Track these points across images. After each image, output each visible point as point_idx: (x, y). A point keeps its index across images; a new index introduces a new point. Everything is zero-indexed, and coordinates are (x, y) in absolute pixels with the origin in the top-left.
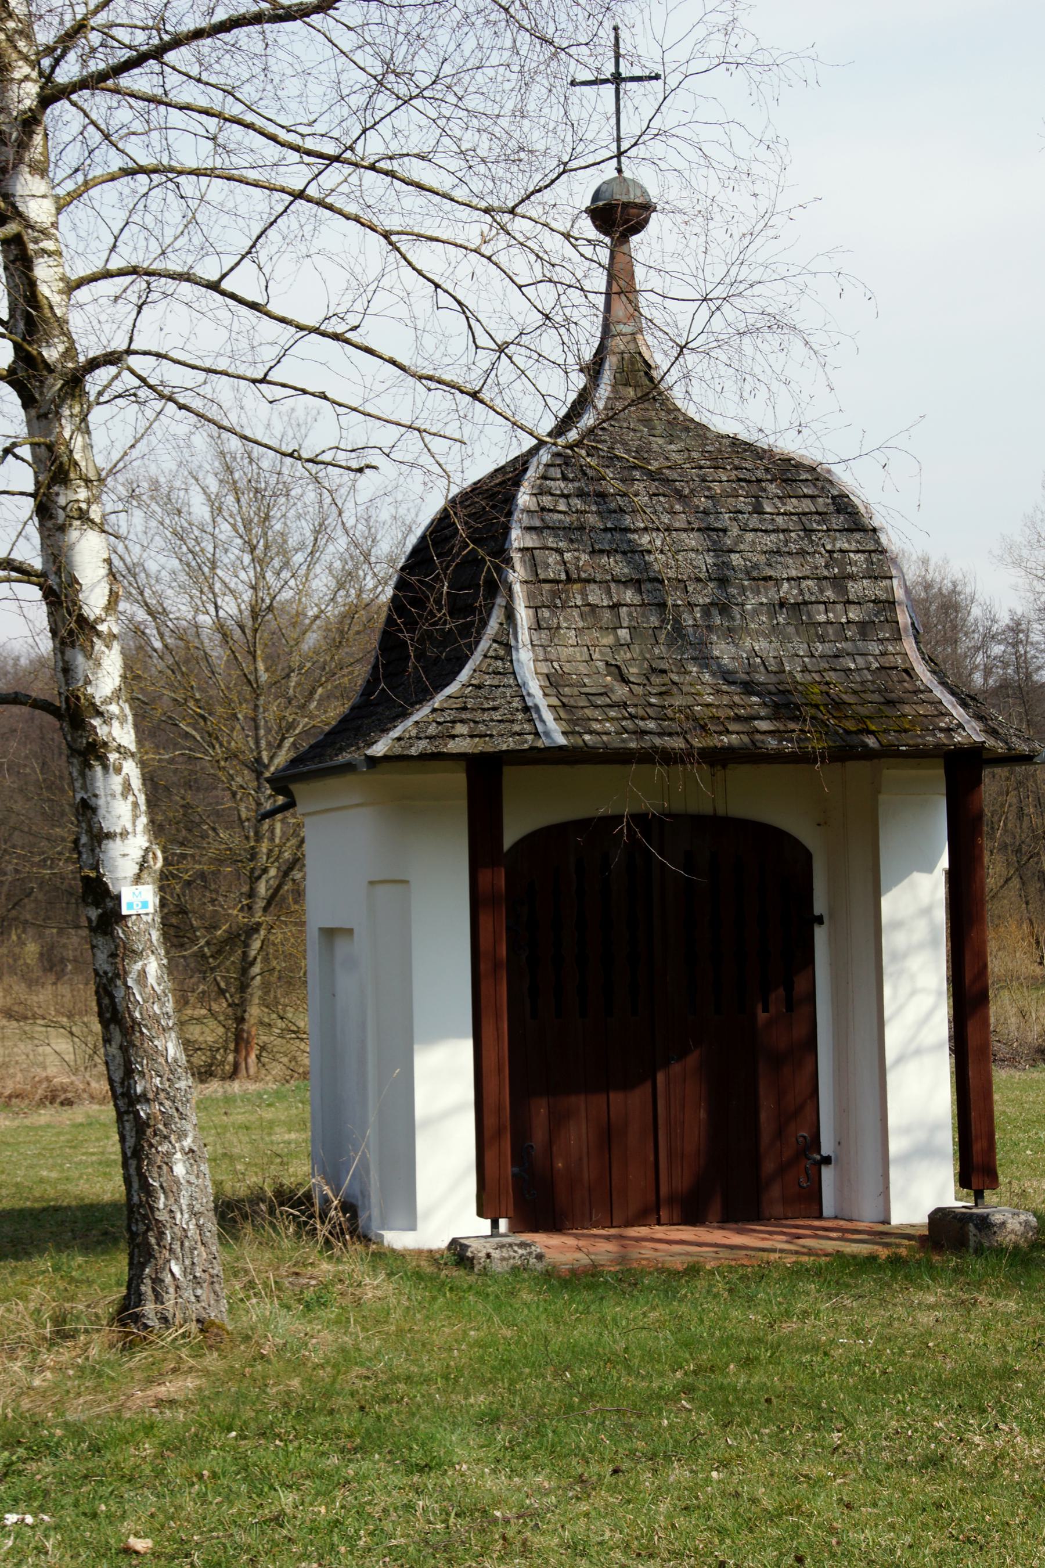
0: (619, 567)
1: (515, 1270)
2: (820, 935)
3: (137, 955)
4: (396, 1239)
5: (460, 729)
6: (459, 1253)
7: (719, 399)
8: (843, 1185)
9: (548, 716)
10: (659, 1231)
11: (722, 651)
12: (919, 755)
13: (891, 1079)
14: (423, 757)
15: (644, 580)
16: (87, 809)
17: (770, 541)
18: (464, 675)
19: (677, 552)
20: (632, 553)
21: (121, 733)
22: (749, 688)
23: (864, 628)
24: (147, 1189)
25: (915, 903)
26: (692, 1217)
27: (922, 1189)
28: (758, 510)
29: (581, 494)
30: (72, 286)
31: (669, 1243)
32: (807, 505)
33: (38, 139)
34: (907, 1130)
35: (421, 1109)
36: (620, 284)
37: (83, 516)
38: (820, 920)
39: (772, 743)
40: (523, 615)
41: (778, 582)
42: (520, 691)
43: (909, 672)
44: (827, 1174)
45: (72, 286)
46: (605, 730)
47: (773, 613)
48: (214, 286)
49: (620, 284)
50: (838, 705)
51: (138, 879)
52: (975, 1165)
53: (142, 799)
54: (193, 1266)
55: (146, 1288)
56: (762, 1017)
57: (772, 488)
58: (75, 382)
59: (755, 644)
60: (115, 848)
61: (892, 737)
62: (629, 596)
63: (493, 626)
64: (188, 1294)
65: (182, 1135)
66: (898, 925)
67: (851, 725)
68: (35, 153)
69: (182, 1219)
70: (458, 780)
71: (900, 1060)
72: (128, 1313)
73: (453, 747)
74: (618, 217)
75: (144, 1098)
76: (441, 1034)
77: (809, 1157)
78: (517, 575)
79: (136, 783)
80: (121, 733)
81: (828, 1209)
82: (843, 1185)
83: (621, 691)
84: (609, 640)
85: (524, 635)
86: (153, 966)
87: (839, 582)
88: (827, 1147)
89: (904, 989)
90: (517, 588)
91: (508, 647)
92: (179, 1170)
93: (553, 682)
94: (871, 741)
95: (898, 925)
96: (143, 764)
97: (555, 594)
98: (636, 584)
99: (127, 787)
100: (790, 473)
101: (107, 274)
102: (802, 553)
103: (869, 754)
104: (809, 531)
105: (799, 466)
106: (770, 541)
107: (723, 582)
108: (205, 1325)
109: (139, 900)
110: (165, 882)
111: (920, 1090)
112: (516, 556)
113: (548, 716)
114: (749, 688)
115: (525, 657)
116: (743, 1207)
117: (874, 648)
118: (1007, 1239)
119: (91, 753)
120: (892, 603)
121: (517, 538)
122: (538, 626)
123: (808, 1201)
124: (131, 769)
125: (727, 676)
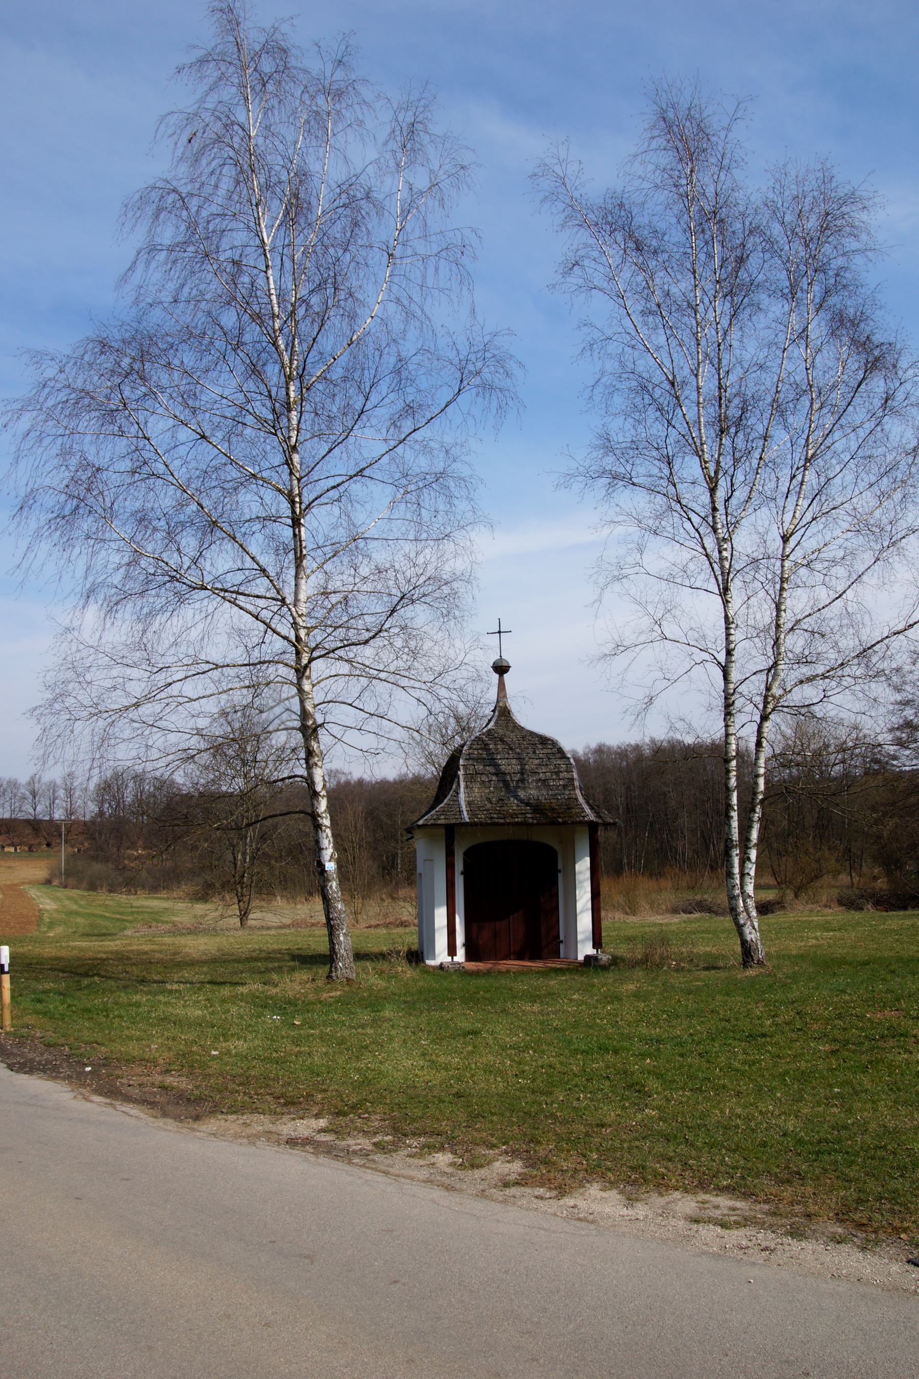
0: (491, 769)
1: (456, 971)
2: (560, 876)
3: (330, 881)
4: (430, 962)
5: (442, 817)
6: (441, 967)
7: (528, 718)
8: (566, 948)
9: (465, 813)
10: (509, 962)
11: (522, 794)
12: (581, 823)
13: (578, 917)
14: (432, 825)
15: (499, 773)
16: (317, 842)
17: (537, 762)
18: (445, 801)
19: (509, 765)
20: (496, 766)
21: (326, 822)
22: (527, 804)
23: (565, 787)
24: (334, 944)
25: (583, 866)
26: (520, 957)
27: (585, 949)
28: (534, 753)
29: (481, 749)
30: (315, 706)
31: (513, 964)
32: (549, 751)
33: (308, 671)
34: (583, 932)
35: (436, 926)
36: (501, 686)
37: (316, 764)
38: (560, 871)
39: (531, 821)
40: (462, 785)
41: (539, 773)
42: (459, 806)
43: (576, 799)
44: (562, 946)
45: (315, 706)
46: (482, 817)
47: (537, 783)
48: (350, 705)
49: (501, 686)
50: (553, 809)
51: (330, 861)
52: (597, 944)
53: (331, 839)
54: (345, 966)
55: (333, 969)
56: (542, 900)
57: (540, 746)
58: (315, 730)
59: (532, 792)
60: (324, 852)
61: (567, 819)
62: (494, 778)
63: (454, 787)
64: (344, 971)
65: (342, 929)
66: (580, 873)
67: (555, 815)
68: (307, 673)
69: (342, 951)
70: (442, 831)
71: (581, 912)
72: (329, 977)
73: (439, 822)
74: (501, 669)
75: (332, 919)
76: (440, 905)
77: (556, 941)
78: (461, 773)
79: (330, 834)
80: (326, 822)
81: (562, 955)
82: (566, 948)
83: (489, 806)
84: (487, 791)
85: (462, 790)
86: (334, 884)
87: (557, 773)
88: (562, 938)
89: (582, 892)
90: (461, 778)
91: (458, 793)
92: (342, 938)
93: (469, 804)
94: (560, 820)
95: (580, 873)
96: (332, 830)
97: (472, 778)
98: (496, 774)
99: (327, 836)
100: (544, 741)
101: (324, 702)
102: (547, 765)
103: (559, 824)
104: (549, 759)
105: (549, 740)
106: (537, 762)
107: (522, 774)
108: (348, 980)
109: (330, 866)
110: (338, 862)
111: (584, 922)
112: (461, 767)
113: (465, 813)
114: (527, 804)
115: (462, 796)
116: (535, 956)
117: (567, 792)
118: (602, 963)
119: (318, 827)
120: (573, 779)
121: (461, 762)
122: (467, 787)
123: (556, 954)
124: (329, 831)
125: (521, 801)
